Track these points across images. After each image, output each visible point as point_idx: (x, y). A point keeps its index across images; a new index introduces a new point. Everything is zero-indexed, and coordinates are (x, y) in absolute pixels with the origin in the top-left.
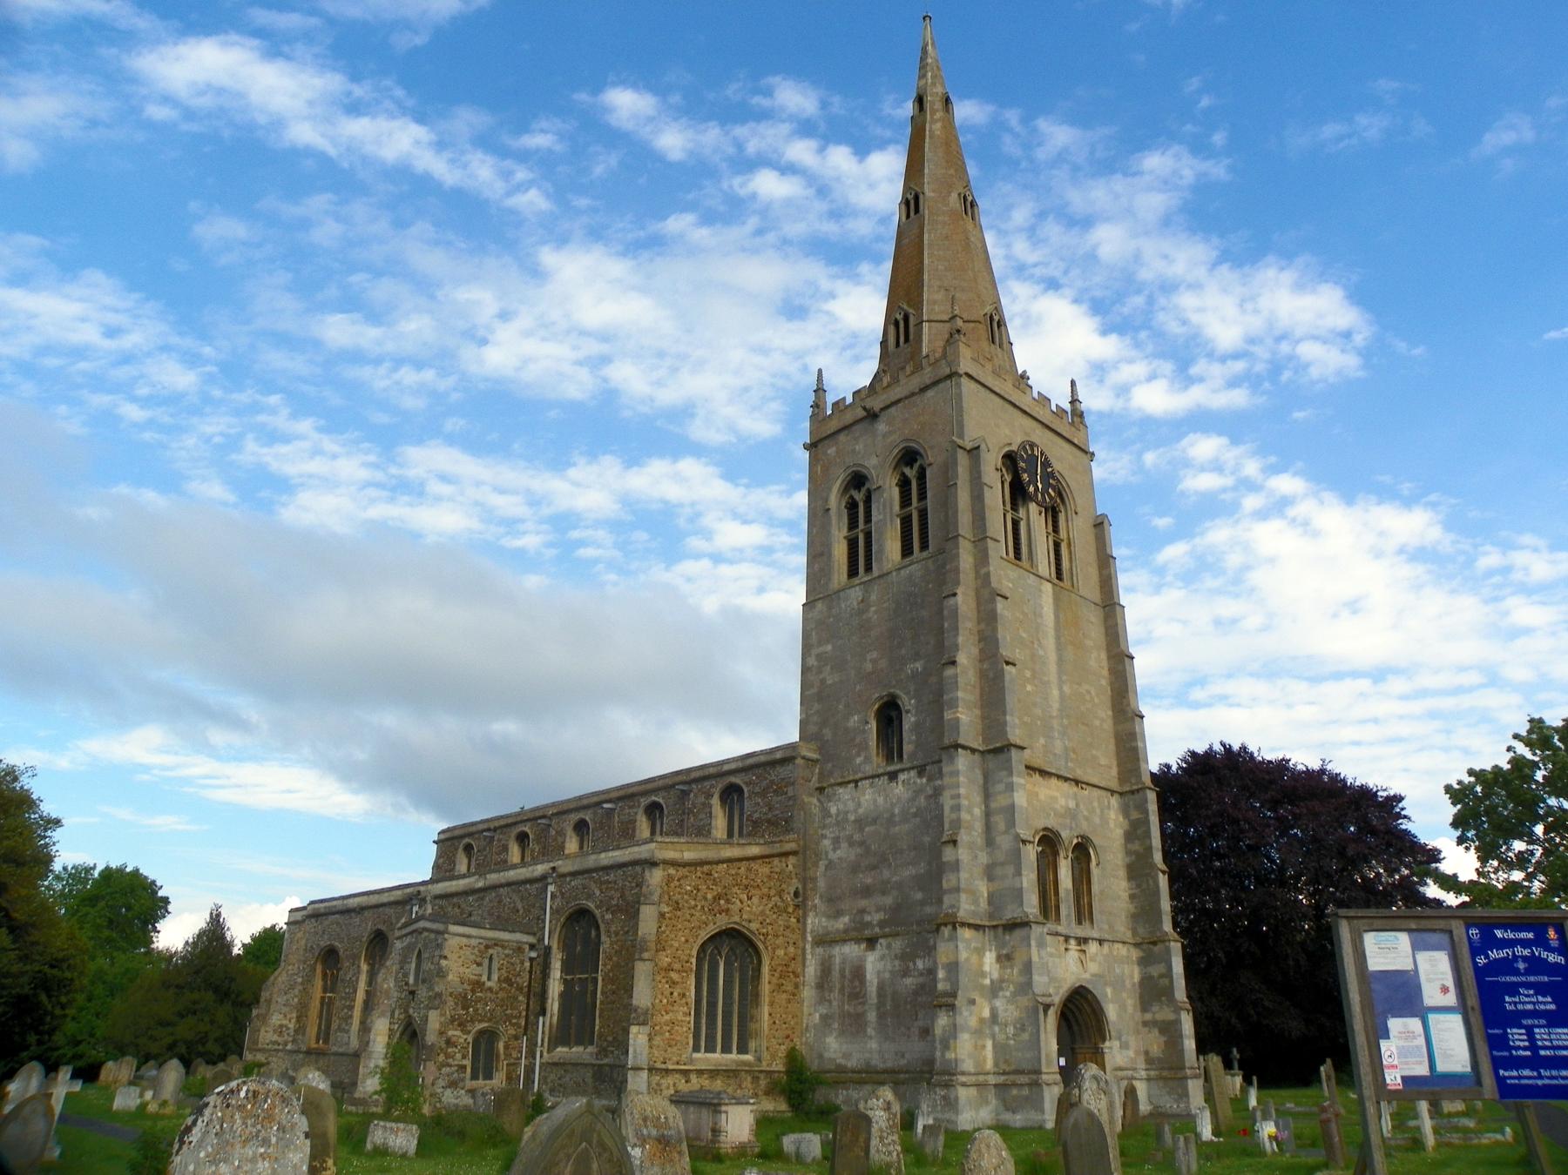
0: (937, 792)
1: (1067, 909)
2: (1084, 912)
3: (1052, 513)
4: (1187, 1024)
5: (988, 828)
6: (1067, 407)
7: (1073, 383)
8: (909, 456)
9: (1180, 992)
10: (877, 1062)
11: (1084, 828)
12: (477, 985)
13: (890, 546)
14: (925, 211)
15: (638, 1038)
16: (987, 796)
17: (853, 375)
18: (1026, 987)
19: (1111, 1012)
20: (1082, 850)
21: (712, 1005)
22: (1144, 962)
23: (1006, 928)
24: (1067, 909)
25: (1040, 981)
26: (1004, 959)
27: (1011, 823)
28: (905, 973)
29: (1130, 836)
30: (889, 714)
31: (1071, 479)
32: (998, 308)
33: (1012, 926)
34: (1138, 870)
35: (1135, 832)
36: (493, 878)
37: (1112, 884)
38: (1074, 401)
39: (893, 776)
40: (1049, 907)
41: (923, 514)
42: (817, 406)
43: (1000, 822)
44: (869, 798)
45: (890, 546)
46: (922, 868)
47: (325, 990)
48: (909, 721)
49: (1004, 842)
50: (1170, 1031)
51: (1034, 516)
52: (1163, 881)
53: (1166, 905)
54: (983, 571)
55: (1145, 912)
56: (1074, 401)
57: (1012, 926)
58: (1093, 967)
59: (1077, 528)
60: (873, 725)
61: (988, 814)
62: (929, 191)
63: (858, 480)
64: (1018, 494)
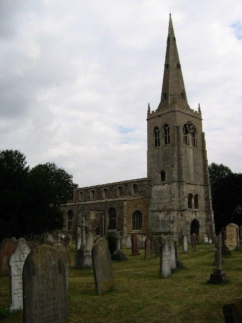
0: (171, 188)
1: (193, 206)
2: (196, 207)
3: (193, 134)
4: (214, 225)
5: (179, 194)
6: (197, 110)
7: (170, 14)
8: (166, 125)
9: (213, 221)
10: (161, 231)
11: (197, 193)
12: (96, 220)
13: (162, 142)
14: (170, 67)
15: (125, 228)
16: (179, 189)
17: (154, 108)
18: (185, 220)
19: (200, 223)
20: (197, 196)
21: (135, 222)
22: (207, 215)
23: (181, 210)
24: (193, 206)
25: (187, 219)
26: (182, 215)
27: (183, 194)
28: (166, 217)
29: (205, 193)
30: (163, 174)
31: (197, 127)
32: (184, 90)
33: (183, 210)
34: (207, 199)
35: (206, 192)
36: (88, 202)
37: (202, 202)
38: (199, 108)
39: (164, 184)
40: (190, 206)
41: (169, 136)
42: (149, 111)
43: (181, 193)
44: (160, 188)
45: (162, 142)
46: (169, 200)
47: (110, 216)
48: (166, 175)
49: (182, 197)
50: (211, 226)
51: (190, 136)
52: (211, 201)
53: (211, 205)
54: (115, 253)
55: (207, 207)
56: (199, 108)
57: (183, 210)
58: (198, 216)
59: (198, 136)
60: (160, 175)
61: (179, 192)
62: (170, 64)
63: (156, 128)
64: (186, 132)
